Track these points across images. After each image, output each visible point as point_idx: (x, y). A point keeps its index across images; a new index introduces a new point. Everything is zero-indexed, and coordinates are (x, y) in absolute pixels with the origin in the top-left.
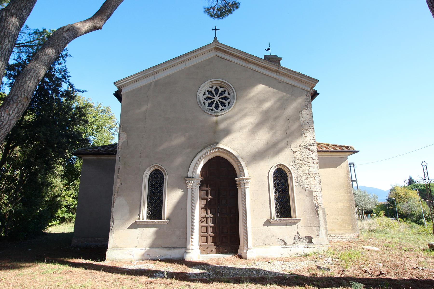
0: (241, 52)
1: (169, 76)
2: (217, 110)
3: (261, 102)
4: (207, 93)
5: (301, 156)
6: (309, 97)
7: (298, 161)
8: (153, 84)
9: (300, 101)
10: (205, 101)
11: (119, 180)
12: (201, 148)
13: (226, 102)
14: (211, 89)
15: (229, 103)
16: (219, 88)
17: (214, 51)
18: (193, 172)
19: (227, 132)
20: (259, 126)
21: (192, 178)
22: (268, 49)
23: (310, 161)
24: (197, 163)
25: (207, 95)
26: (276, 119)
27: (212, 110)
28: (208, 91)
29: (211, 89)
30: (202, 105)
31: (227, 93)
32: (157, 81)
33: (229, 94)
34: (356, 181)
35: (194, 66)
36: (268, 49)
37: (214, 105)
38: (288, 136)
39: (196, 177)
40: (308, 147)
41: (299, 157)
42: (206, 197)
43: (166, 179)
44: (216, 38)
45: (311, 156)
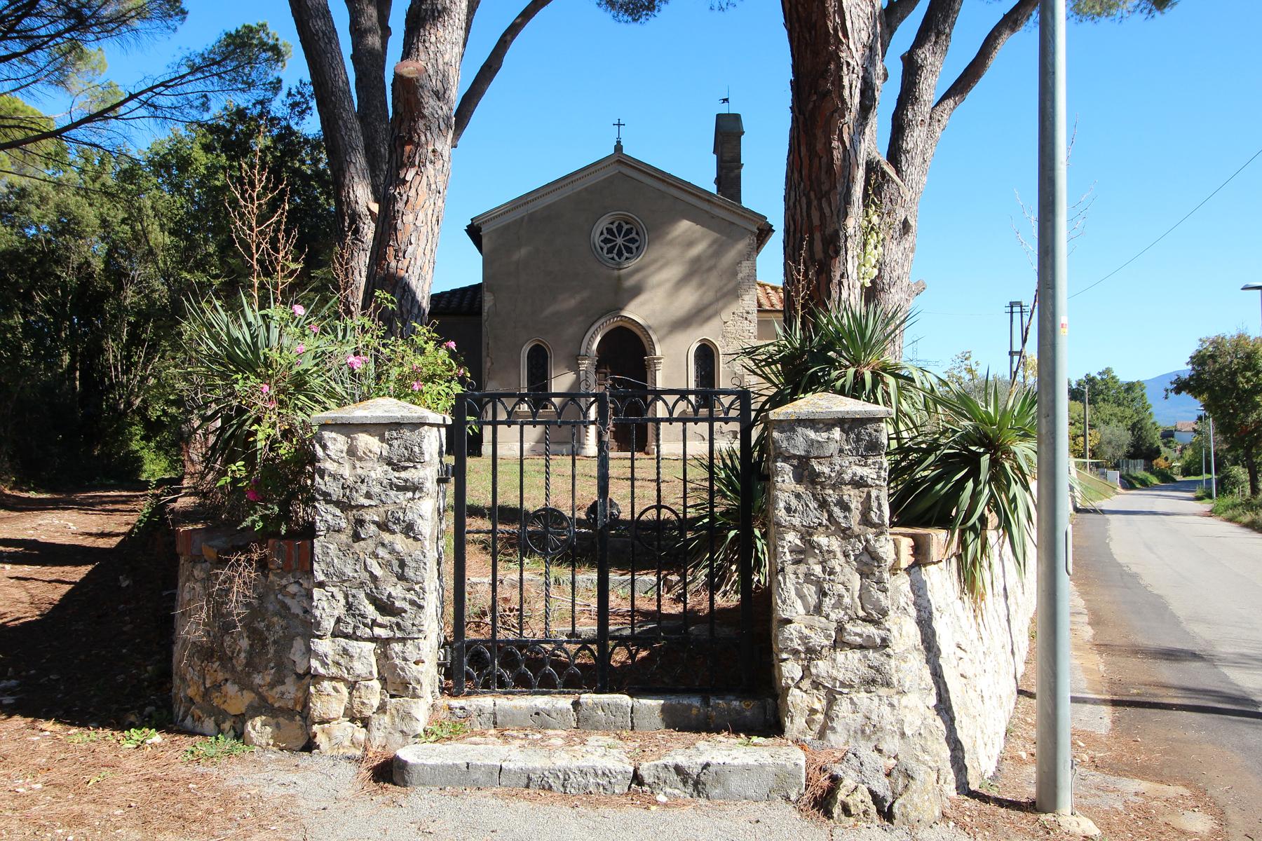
1: (549, 206)
3: (690, 244)
4: (605, 232)
10: (602, 244)
11: (488, 359)
13: (634, 246)
14: (611, 226)
15: (637, 248)
16: (624, 224)
19: (636, 291)
21: (586, 356)
22: (726, 100)
23: (746, 334)
25: (606, 235)
26: (710, 269)
27: (613, 259)
29: (611, 226)
31: (634, 232)
32: (531, 214)
35: (586, 189)
36: (726, 100)
37: (615, 251)
38: (724, 295)
40: (745, 315)
41: (730, 329)
44: (618, 147)
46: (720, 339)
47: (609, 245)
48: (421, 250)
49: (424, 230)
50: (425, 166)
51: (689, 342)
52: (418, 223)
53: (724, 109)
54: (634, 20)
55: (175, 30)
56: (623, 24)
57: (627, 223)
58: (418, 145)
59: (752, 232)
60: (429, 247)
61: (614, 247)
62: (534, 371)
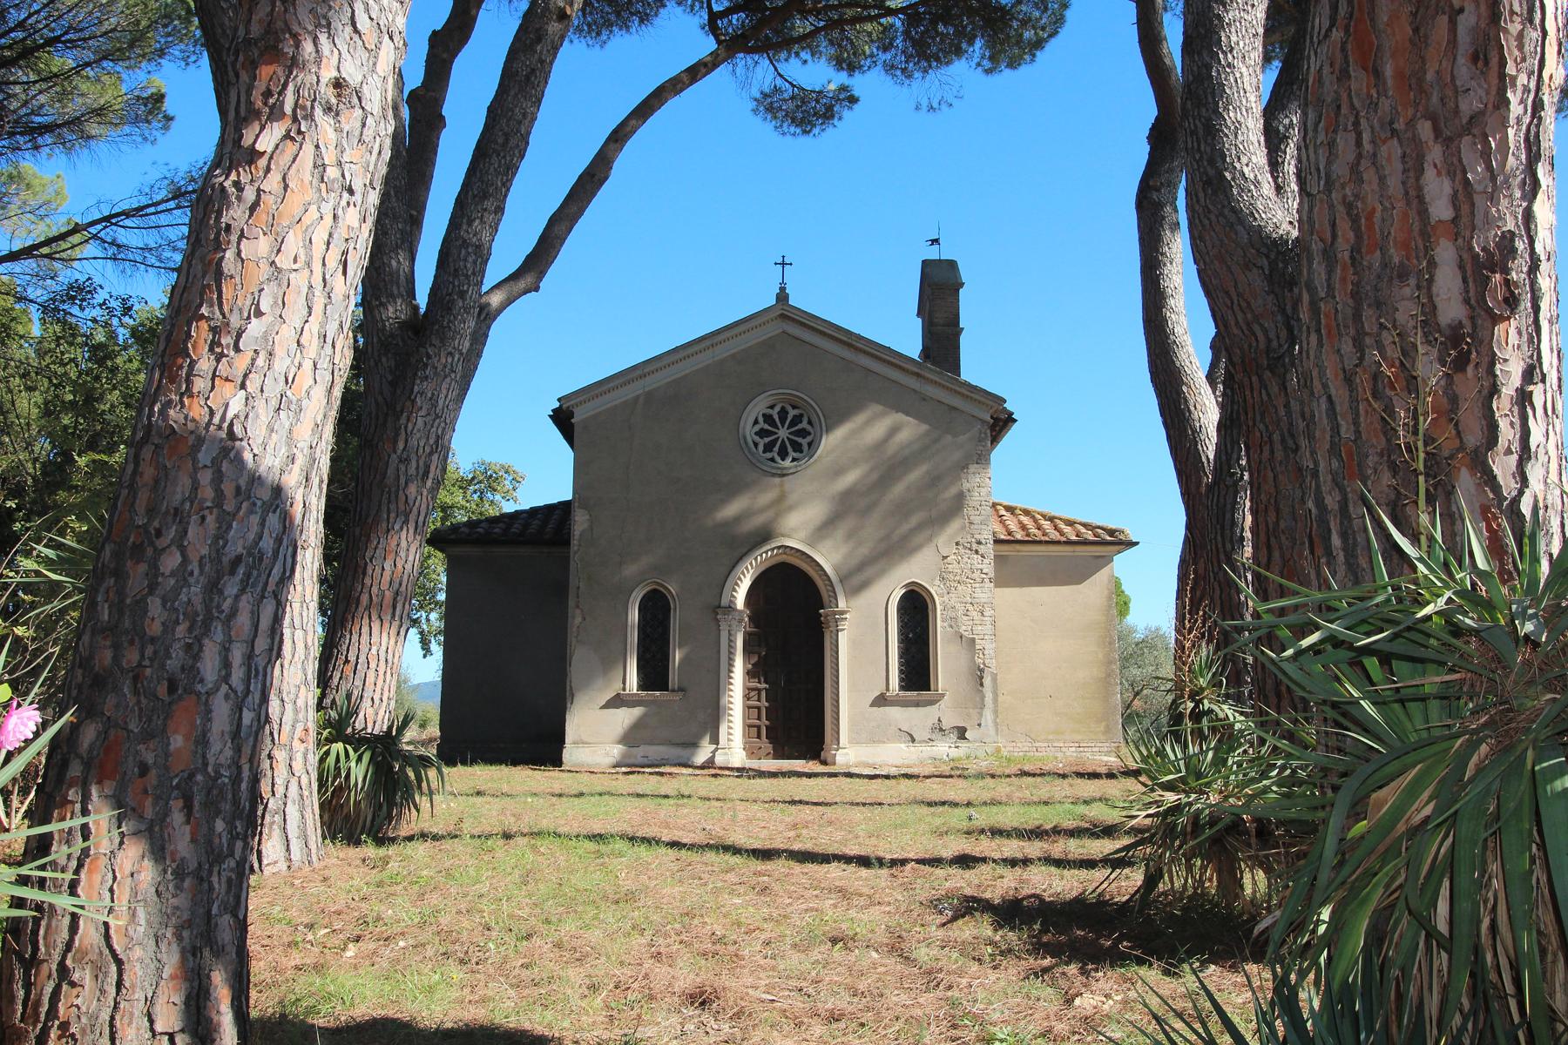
4: (761, 419)
8: (641, 400)
10: (757, 439)
11: (578, 612)
13: (804, 442)
14: (770, 411)
15: (810, 444)
16: (789, 409)
22: (935, 241)
23: (977, 575)
25: (762, 425)
28: (764, 415)
33: (810, 423)
35: (733, 356)
36: (935, 241)
37: (776, 449)
40: (975, 546)
41: (955, 567)
44: (782, 296)
45: (980, 566)
46: (937, 582)
47: (767, 440)
48: (287, 334)
49: (299, 280)
50: (310, 117)
51: (889, 591)
52: (284, 261)
53: (933, 254)
54: (806, 132)
55: (154, 142)
56: (789, 138)
57: (794, 407)
58: (294, 64)
59: (983, 421)
60: (314, 326)
61: (773, 443)
62: (649, 630)
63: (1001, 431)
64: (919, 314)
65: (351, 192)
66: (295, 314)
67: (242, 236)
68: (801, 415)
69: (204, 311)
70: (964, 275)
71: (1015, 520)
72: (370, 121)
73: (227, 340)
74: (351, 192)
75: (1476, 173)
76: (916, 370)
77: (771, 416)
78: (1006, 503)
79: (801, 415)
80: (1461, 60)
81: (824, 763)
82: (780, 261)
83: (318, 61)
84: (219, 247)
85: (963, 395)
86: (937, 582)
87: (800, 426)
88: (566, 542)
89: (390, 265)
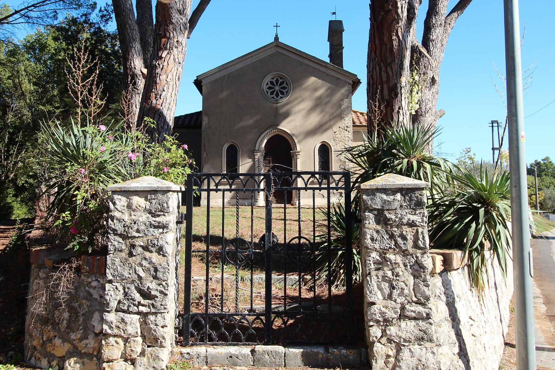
0: (297, 50)
2: (277, 98)
3: (316, 89)
4: (269, 83)
5: (339, 135)
6: (350, 88)
7: (337, 139)
8: (226, 76)
9: (343, 91)
10: (268, 90)
11: (205, 152)
12: (265, 129)
13: (285, 91)
14: (272, 80)
15: (287, 92)
16: (279, 79)
17: (275, 47)
18: (259, 146)
19: (286, 115)
20: (313, 109)
21: (258, 151)
22: (334, 13)
23: (347, 138)
24: (262, 140)
25: (269, 85)
27: (273, 98)
28: (270, 82)
29: (272, 80)
30: (265, 94)
31: (285, 83)
33: (287, 84)
34: (493, 149)
35: (259, 60)
36: (334, 13)
37: (275, 94)
39: (262, 150)
40: (346, 128)
41: (338, 136)
42: (268, 165)
43: (239, 151)
44: (276, 38)
45: (348, 135)
47: (271, 90)
48: (169, 94)
49: (171, 83)
50: (172, 49)
51: (315, 143)
52: (168, 80)
53: (333, 18)
57: (281, 79)
59: (349, 83)
60: (174, 93)
63: (356, 86)
64: (328, 41)
65: (180, 63)
66: (170, 91)
67: (160, 75)
68: (284, 82)
69: (153, 90)
70: (345, 27)
71: (363, 118)
72: (184, 48)
73: (158, 97)
74: (180, 63)
75: (390, 73)
76: (324, 65)
77: (273, 82)
78: (360, 111)
79: (284, 82)
80: (388, 53)
81: (292, 205)
82: (276, 25)
83: (174, 38)
84: (156, 77)
85: (342, 74)
86: (332, 141)
87: (283, 85)
88: (200, 127)
89: (148, 41)
